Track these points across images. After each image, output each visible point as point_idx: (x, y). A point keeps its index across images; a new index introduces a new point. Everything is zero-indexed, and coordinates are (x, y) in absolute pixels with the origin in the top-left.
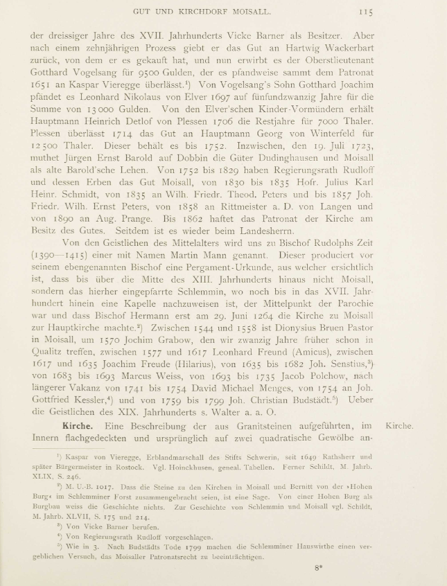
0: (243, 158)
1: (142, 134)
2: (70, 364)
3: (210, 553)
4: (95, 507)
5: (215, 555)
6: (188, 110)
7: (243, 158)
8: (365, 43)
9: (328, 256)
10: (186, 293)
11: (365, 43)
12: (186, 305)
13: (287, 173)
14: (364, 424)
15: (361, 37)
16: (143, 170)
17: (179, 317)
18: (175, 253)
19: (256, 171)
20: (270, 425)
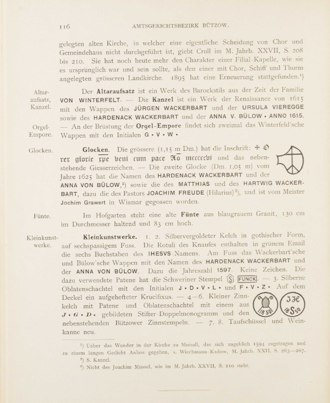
0: (148, 314)
1: (236, 158)
2: (148, 224)
3: (144, 180)
4: (203, 305)
5: (62, 60)
6: (63, 273)
7: (148, 314)
8: (42, 97)
9: (177, 323)
10: (255, 69)
11: (42, 97)
12: (188, 26)
13: (109, 218)
14: (111, 201)
15: (38, 93)
16: (284, 270)
17: (152, 92)
18: (229, 49)
19: (120, 255)
20: (65, 167)
